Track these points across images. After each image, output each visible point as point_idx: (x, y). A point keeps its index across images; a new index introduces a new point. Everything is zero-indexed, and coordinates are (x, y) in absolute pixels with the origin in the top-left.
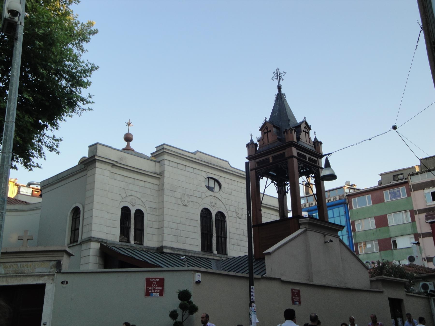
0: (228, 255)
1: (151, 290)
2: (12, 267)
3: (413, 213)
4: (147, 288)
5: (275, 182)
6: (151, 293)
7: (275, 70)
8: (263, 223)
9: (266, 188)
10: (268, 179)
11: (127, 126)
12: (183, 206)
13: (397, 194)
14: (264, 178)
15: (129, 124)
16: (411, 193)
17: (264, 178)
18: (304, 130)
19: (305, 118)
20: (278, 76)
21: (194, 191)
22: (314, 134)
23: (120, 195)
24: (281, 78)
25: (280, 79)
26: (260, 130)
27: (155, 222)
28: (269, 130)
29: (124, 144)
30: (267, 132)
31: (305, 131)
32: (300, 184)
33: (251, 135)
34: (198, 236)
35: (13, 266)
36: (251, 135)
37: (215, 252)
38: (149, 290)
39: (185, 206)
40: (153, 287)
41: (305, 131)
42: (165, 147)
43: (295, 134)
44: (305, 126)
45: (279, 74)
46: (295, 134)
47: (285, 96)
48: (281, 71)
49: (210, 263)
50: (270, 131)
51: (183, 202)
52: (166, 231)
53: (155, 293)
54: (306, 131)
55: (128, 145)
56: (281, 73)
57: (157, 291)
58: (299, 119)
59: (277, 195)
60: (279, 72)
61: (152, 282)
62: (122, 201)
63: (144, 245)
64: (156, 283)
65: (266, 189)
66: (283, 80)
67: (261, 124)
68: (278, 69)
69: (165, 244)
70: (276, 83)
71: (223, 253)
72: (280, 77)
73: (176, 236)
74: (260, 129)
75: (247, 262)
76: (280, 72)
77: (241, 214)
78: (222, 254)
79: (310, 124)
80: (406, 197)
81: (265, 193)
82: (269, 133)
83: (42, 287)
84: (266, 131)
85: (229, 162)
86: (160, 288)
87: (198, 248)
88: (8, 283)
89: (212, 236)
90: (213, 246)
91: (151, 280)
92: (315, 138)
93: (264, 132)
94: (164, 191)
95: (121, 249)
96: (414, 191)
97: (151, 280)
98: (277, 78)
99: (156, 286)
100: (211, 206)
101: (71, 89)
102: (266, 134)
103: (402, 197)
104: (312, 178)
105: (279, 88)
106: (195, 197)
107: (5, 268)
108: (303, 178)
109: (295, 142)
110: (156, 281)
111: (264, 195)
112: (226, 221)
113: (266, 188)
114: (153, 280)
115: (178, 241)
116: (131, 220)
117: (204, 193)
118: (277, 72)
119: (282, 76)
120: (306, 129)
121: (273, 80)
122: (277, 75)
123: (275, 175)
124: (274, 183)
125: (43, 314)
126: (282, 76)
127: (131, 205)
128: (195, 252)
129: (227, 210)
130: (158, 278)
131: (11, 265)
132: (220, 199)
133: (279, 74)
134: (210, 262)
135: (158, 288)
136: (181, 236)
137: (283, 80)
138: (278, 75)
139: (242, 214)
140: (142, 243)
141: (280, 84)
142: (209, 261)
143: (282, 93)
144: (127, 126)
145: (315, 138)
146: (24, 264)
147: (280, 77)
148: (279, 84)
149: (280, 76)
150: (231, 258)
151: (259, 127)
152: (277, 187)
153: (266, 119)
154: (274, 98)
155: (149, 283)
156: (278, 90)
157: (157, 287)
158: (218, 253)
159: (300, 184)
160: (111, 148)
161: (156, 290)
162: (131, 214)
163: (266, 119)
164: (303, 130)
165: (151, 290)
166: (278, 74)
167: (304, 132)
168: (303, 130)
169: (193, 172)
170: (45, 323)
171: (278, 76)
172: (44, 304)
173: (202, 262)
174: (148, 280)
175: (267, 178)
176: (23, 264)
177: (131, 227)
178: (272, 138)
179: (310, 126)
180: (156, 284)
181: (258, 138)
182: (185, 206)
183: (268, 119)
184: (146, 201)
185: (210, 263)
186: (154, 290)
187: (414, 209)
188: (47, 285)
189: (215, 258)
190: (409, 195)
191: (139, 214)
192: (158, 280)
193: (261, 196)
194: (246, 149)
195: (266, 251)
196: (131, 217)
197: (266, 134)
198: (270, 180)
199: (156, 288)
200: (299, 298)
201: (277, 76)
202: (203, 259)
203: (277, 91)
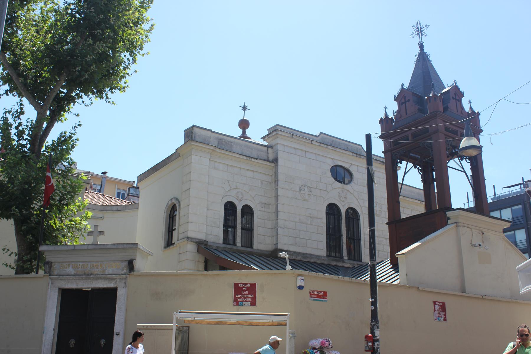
0: (363, 261)
1: (240, 298)
2: (82, 268)
4: (235, 296)
5: (419, 167)
6: (240, 301)
7: (415, 24)
8: (401, 218)
9: (405, 174)
10: (408, 163)
11: (243, 110)
12: (303, 200)
14: (403, 162)
15: (244, 108)
17: (403, 162)
18: (454, 97)
19: (455, 81)
20: (420, 31)
21: (317, 183)
22: (469, 103)
23: (223, 187)
24: (424, 34)
25: (422, 34)
26: (395, 100)
27: (267, 220)
28: (407, 99)
29: (239, 132)
30: (405, 102)
31: (455, 99)
32: (448, 168)
33: (386, 107)
34: (323, 238)
35: (83, 266)
36: (386, 107)
37: (346, 258)
38: (238, 298)
39: (306, 200)
40: (243, 294)
41: (455, 99)
42: (278, 127)
43: (440, 102)
44: (455, 92)
45: (421, 28)
46: (440, 102)
47: (428, 56)
48: (423, 25)
49: (338, 270)
50: (409, 101)
51: (302, 196)
52: (280, 231)
53: (246, 301)
54: (457, 98)
55: (244, 132)
56: (423, 27)
57: (247, 299)
58: (447, 83)
59: (421, 186)
60: (420, 25)
61: (242, 288)
62: (226, 194)
63: (254, 248)
64: (247, 289)
65: (405, 175)
66: (426, 36)
67: (396, 92)
68: (419, 22)
69: (279, 247)
70: (417, 40)
71: (356, 259)
72: (422, 32)
73: (293, 237)
74: (395, 98)
75: (377, 268)
76: (421, 26)
77: (379, 211)
78: (354, 260)
79: (462, 89)
81: (403, 183)
82: (407, 103)
83: (113, 292)
84: (403, 101)
85: (362, 146)
86: (251, 296)
87: (323, 252)
88: (78, 285)
89: (341, 237)
90: (343, 250)
91: (240, 285)
92: (471, 108)
93: (401, 103)
94: (278, 182)
95: (223, 252)
97: (240, 285)
98: (418, 34)
99: (247, 292)
100: (339, 201)
102: (404, 105)
104: (467, 160)
105: (421, 46)
106: (319, 189)
107: (74, 268)
108: (455, 161)
109: (441, 112)
110: (247, 287)
111: (403, 185)
112: (360, 219)
113: (405, 174)
114: (243, 285)
115: (296, 244)
116: (238, 218)
117: (330, 185)
118: (418, 26)
119: (424, 30)
120: (457, 96)
121: (413, 37)
122: (417, 30)
123: (419, 157)
124: (418, 169)
125: (116, 322)
126: (424, 30)
127: (237, 200)
128: (318, 257)
129: (360, 205)
130: (249, 284)
131: (80, 265)
132: (352, 192)
133: (421, 28)
134: (339, 269)
135: (249, 296)
136: (301, 237)
137: (426, 36)
138: (419, 30)
139: (381, 211)
140: (251, 246)
141: (422, 42)
142: (337, 268)
143: (425, 52)
144: (243, 110)
145: (471, 108)
146: (94, 264)
147: (421, 31)
148: (421, 41)
149: (422, 31)
150: (365, 265)
151: (395, 97)
152: (421, 173)
153: (403, 85)
154: (414, 60)
155: (238, 289)
156: (419, 49)
157: (248, 294)
158: (349, 259)
159: (448, 168)
160: (211, 131)
161: (247, 298)
162: (238, 211)
163: (403, 85)
164: (453, 97)
165: (240, 298)
166: (419, 29)
167: (454, 100)
168: (453, 97)
169: (315, 159)
170: (118, 333)
171: (420, 31)
172: (116, 311)
173: (319, 268)
174: (236, 285)
175: (406, 162)
176: (93, 264)
177: (238, 227)
178: (412, 108)
179: (462, 92)
180: (247, 291)
181: (395, 112)
182: (306, 200)
183: (407, 85)
184: (256, 195)
185: (338, 270)
186: (244, 298)
188: (118, 289)
189: (345, 265)
191: (248, 211)
192: (249, 286)
193: (400, 186)
194: (379, 126)
195: (400, 252)
196: (237, 213)
197: (404, 105)
198: (410, 165)
199: (246, 296)
200: (444, 313)
201: (417, 31)
202: (323, 266)
203: (418, 50)
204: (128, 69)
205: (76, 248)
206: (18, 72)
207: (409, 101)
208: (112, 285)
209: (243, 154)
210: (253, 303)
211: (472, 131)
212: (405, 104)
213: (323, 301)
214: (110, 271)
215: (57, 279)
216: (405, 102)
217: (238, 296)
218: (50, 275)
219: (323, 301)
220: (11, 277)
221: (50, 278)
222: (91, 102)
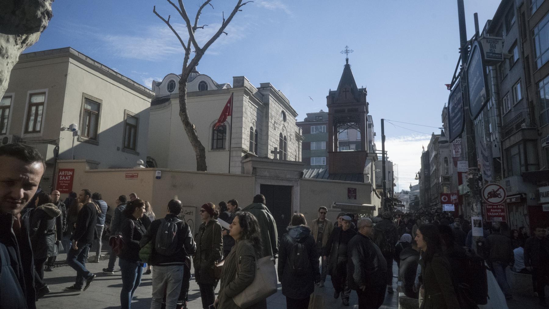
50: (348, 91)
65: (386, 143)
70: (344, 56)
83: (290, 188)
102: (345, 93)
105: (347, 60)
155: (349, 190)
174: (349, 188)
192: (354, 189)
205: (380, 183)
207: (348, 91)
208: (290, 184)
210: (355, 198)
211: (501, 162)
214: (288, 176)
215: (259, 178)
216: (346, 91)
217: (490, 215)
218: (256, 176)
220: (219, 174)
221: (255, 177)
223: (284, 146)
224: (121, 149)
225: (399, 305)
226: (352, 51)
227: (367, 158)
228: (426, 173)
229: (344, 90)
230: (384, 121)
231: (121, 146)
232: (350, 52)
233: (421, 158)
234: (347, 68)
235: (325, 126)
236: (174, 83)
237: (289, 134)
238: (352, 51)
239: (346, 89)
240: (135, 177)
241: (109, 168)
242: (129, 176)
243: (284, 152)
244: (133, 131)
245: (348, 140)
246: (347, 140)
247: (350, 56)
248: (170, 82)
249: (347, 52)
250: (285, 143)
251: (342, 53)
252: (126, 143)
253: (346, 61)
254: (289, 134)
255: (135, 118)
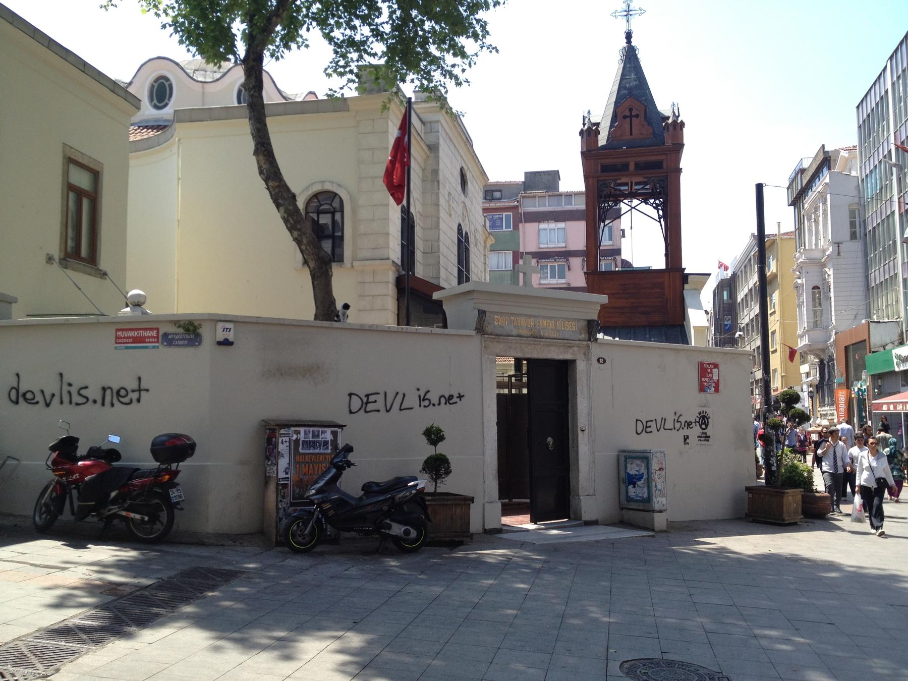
3: (517, 256)
13: (498, 223)
16: (520, 225)
28: (634, 113)
30: (631, 117)
47: (637, 52)
50: (637, 116)
56: (635, 9)
70: (621, 27)
80: (511, 229)
96: (525, 222)
101: (359, 15)
102: (628, 119)
103: (504, 229)
105: (629, 36)
126: (621, 12)
187: (521, 250)
190: (516, 227)
197: (628, 119)
204: (826, 149)
206: (350, 36)
208: (568, 356)
209: (557, 197)
212: (631, 121)
213: (147, 347)
216: (631, 117)
219: (147, 347)
222: (167, 26)
223: (827, 223)
224: (57, 260)
225: (459, 554)
226: (642, 11)
227: (686, 286)
228: (727, 325)
229: (627, 113)
230: (765, 190)
231: (56, 253)
232: (635, 14)
233: (714, 292)
234: (630, 57)
235: (511, 213)
236: (167, 84)
237: (472, 230)
238: (642, 11)
239: (631, 110)
240: (147, 340)
241: (28, 315)
242: (129, 337)
243: (465, 273)
244: (85, 203)
245: (613, 245)
246: (610, 245)
247: (636, 25)
248: (156, 81)
249: (628, 13)
250: (467, 250)
251: (616, 17)
252: (70, 243)
253: (626, 38)
254: (472, 230)
255: (90, 172)
